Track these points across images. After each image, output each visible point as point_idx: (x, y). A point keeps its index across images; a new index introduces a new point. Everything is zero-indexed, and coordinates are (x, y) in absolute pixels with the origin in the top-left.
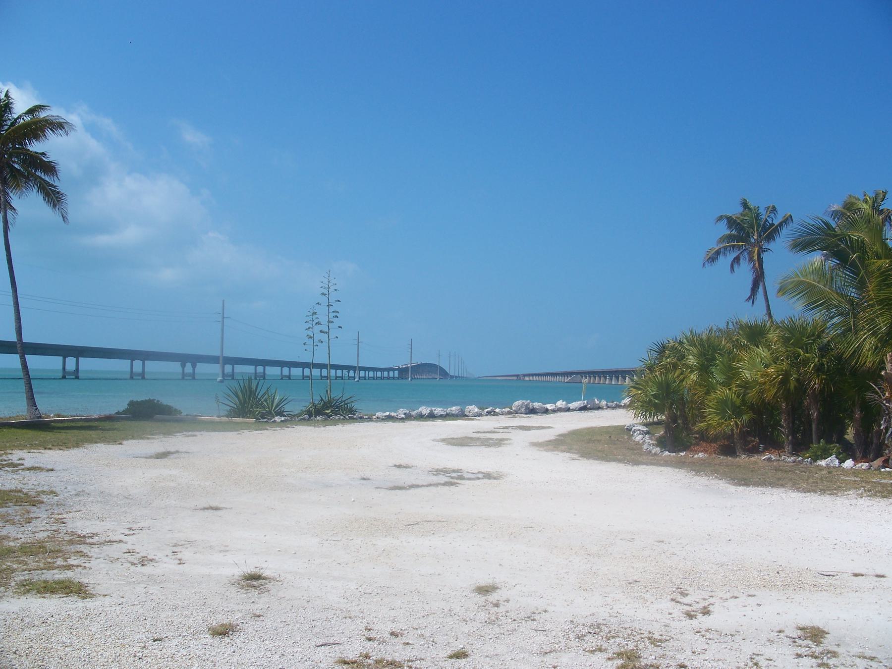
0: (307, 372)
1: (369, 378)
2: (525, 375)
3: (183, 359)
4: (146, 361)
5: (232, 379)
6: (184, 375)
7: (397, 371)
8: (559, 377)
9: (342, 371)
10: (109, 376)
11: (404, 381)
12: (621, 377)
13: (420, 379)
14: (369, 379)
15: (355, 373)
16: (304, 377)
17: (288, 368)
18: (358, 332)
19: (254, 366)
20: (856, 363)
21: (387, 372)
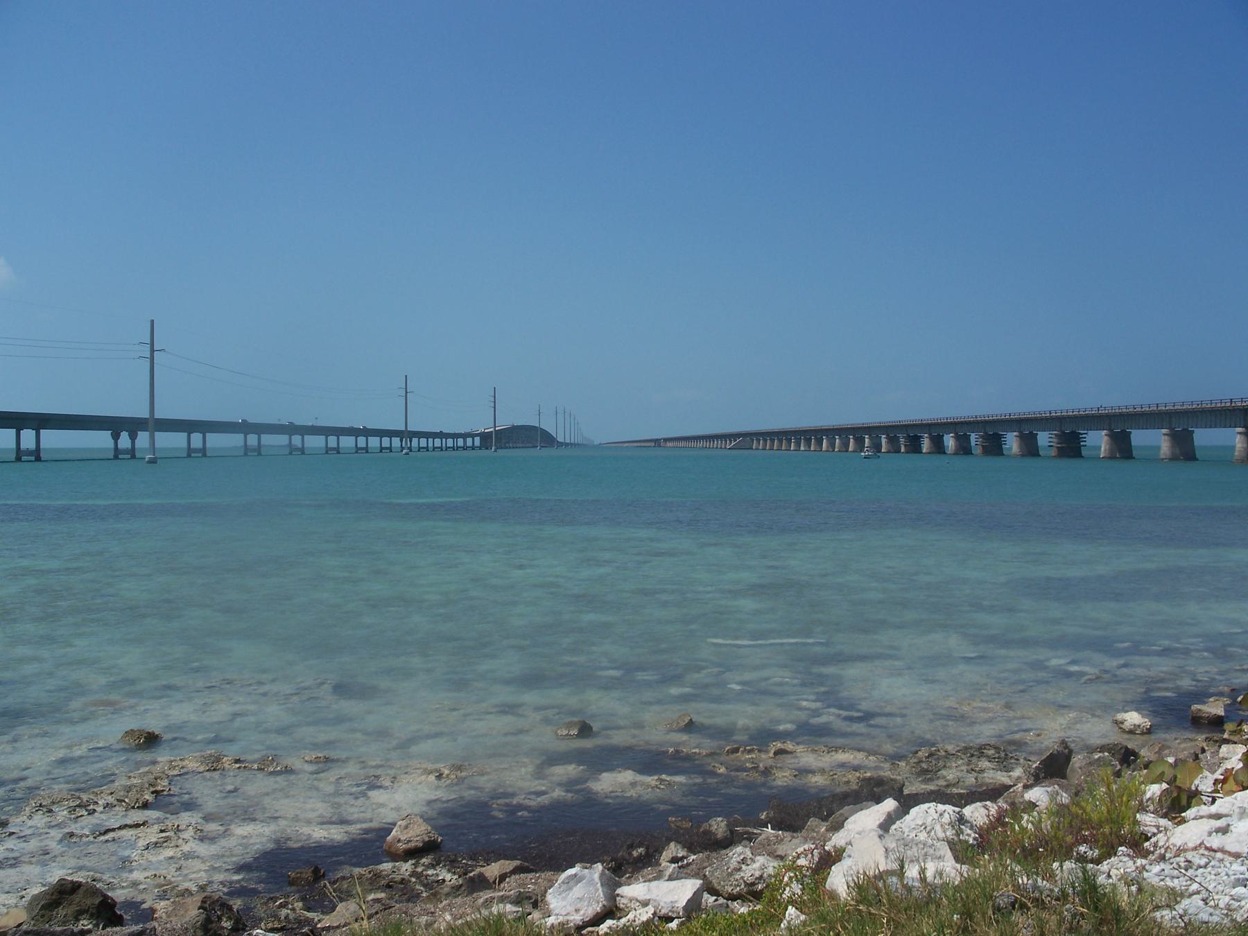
0: (362, 441)
1: (447, 448)
2: (666, 440)
3: (114, 425)
4: (207, 434)
5: (302, 454)
6: (117, 452)
7: (479, 438)
9: (428, 440)
10: (71, 456)
11: (484, 452)
13: (513, 448)
15: (401, 441)
16: (358, 449)
17: (257, 436)
18: (406, 376)
21: (471, 439)
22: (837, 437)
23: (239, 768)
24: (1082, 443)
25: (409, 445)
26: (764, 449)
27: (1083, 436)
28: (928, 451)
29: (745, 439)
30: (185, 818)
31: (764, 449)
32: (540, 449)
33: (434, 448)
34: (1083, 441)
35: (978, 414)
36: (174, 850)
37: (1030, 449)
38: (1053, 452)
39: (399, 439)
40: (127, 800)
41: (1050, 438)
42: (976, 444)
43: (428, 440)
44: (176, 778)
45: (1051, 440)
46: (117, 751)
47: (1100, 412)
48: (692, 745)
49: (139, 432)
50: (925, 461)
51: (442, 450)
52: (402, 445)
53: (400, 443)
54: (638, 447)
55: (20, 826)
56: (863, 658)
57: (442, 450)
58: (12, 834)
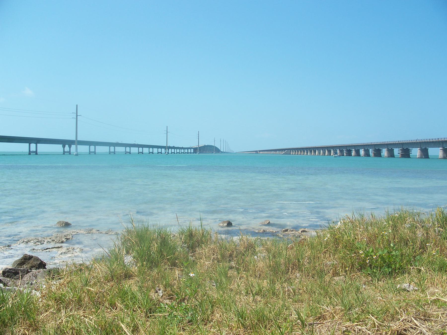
2: (260, 151)
3: (63, 142)
4: (38, 144)
6: (64, 152)
7: (193, 149)
8: (278, 152)
9: (174, 150)
11: (194, 154)
12: (317, 151)
13: (205, 153)
14: (181, 153)
15: (165, 150)
18: (167, 126)
19: (125, 147)
20: (410, 149)
22: (321, 150)
23: (99, 233)
24: (410, 153)
25: (168, 152)
26: (295, 154)
27: (411, 150)
28: (354, 155)
29: (288, 151)
30: (76, 246)
31: (295, 154)
32: (215, 153)
33: (177, 153)
34: (411, 153)
35: (372, 142)
36: (71, 254)
37: (391, 154)
38: (400, 156)
39: (164, 149)
40: (55, 240)
41: (398, 150)
42: (372, 153)
43: (174, 150)
44: (75, 235)
45: (399, 151)
46: (54, 228)
47: (417, 141)
48: (270, 229)
49: (72, 145)
50: (353, 158)
51: (180, 153)
52: (165, 152)
53: (165, 151)
54: (250, 153)
55: (16, 247)
56: (332, 208)
57: (180, 153)
58: (11, 249)
